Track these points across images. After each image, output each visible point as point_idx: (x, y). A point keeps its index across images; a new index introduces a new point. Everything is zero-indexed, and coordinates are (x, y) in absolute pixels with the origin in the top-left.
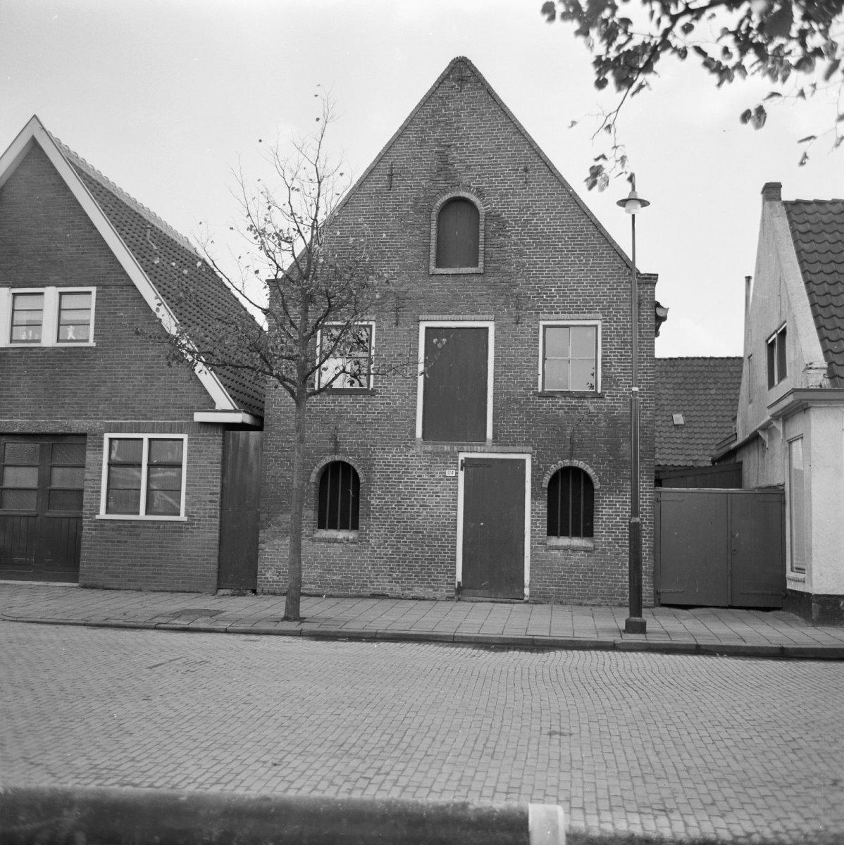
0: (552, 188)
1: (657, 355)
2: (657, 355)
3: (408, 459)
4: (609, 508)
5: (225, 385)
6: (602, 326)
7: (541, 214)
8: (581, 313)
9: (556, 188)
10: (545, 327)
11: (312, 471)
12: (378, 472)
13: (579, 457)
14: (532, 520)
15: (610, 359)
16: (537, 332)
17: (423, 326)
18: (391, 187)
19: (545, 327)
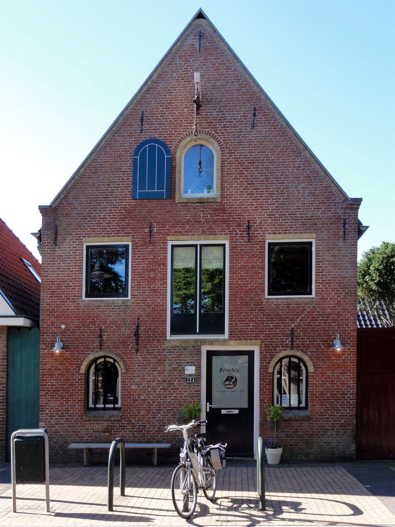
0: (275, 131)
1: (247, 356)
2: (247, 356)
3: (161, 352)
4: (321, 387)
5: (7, 296)
6: (316, 243)
7: (267, 153)
8: (289, 233)
9: (278, 131)
10: (173, 246)
11: (81, 364)
12: (136, 363)
13: (298, 348)
14: (260, 398)
15: (322, 270)
16: (165, 249)
17: (85, 245)
18: (142, 130)
19: (173, 246)
